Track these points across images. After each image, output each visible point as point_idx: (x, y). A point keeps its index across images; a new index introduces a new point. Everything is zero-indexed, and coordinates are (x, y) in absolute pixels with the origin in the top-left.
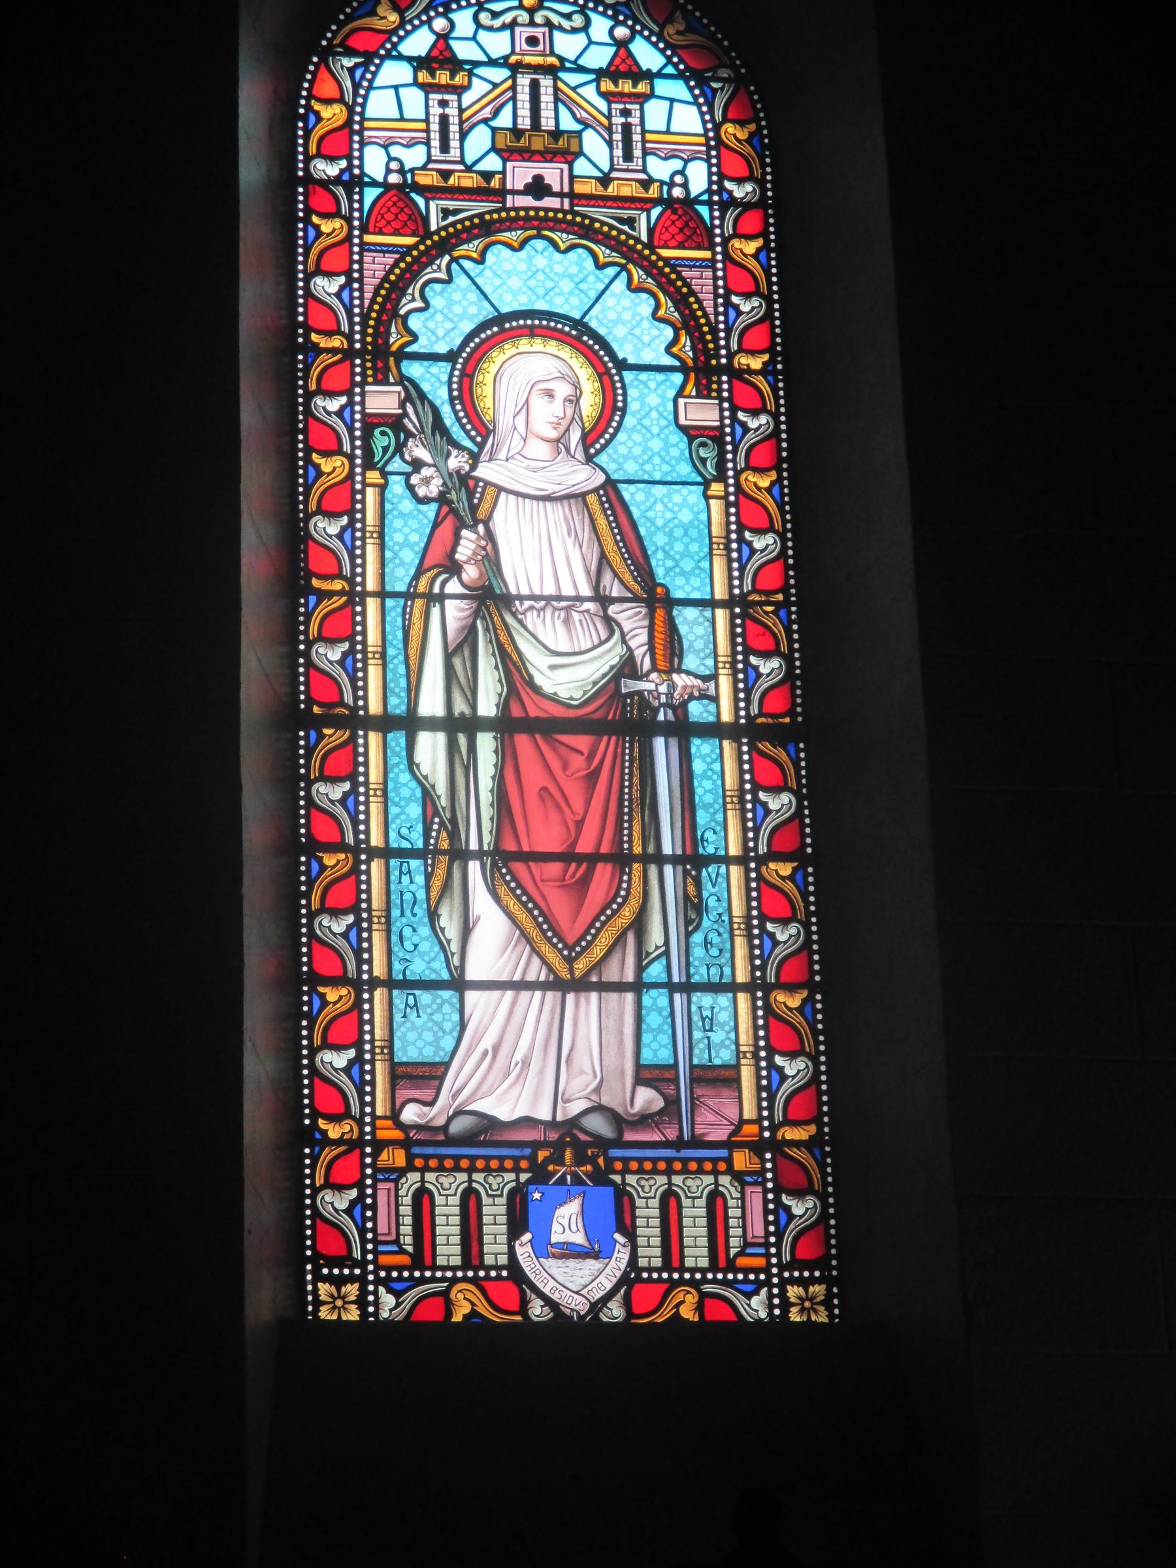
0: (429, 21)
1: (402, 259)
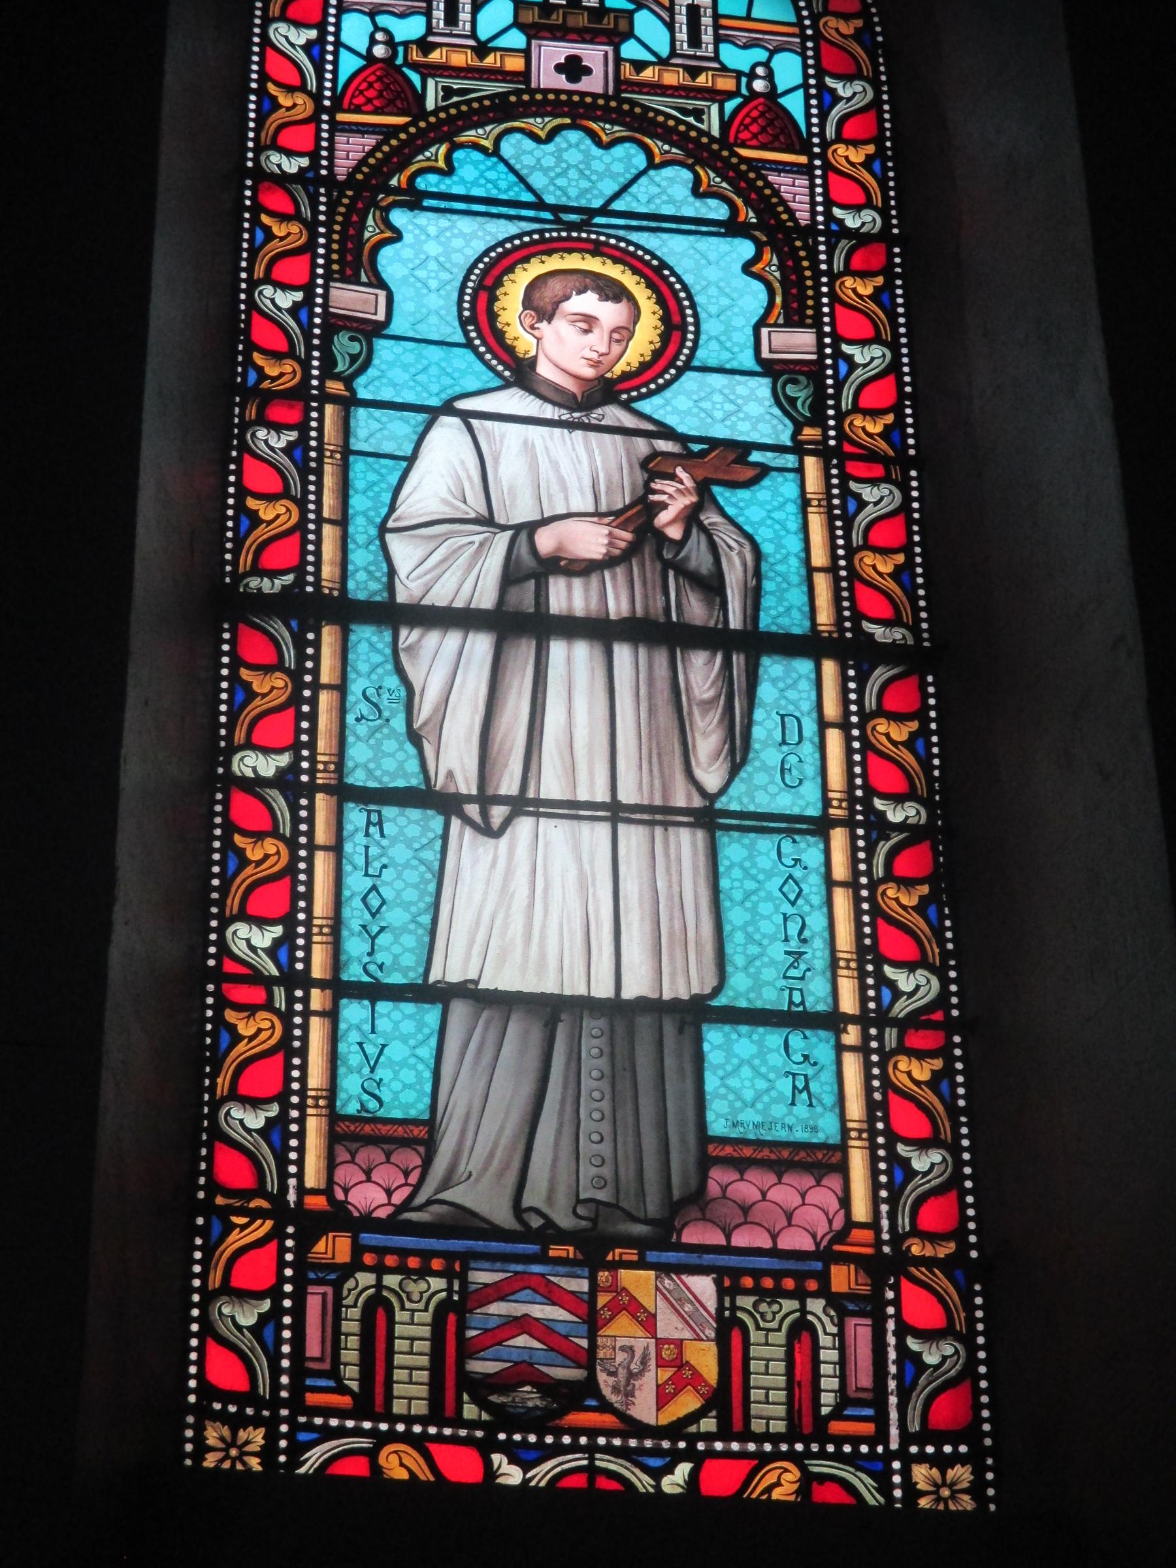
1: (386, 141)
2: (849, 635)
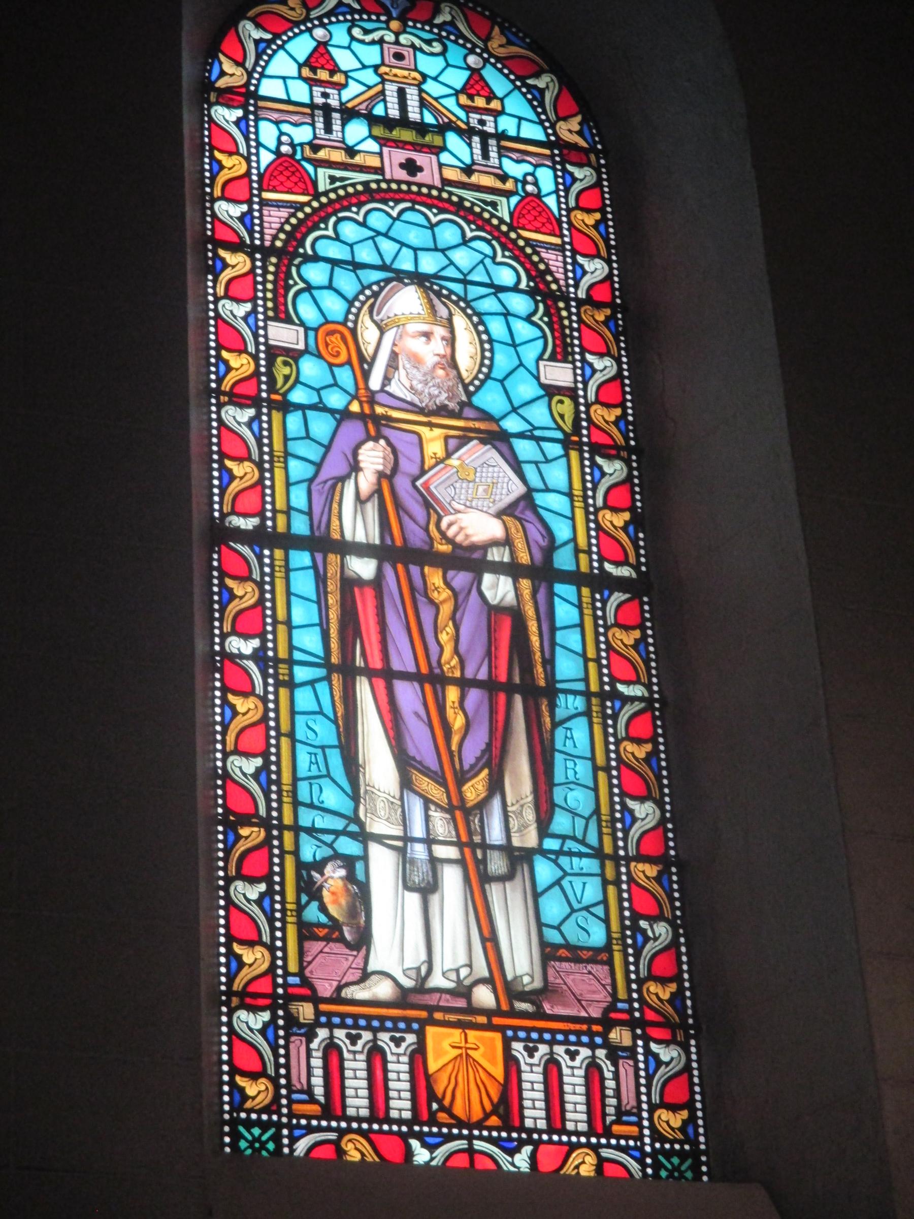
0: (310, 30)
2: (596, 571)
